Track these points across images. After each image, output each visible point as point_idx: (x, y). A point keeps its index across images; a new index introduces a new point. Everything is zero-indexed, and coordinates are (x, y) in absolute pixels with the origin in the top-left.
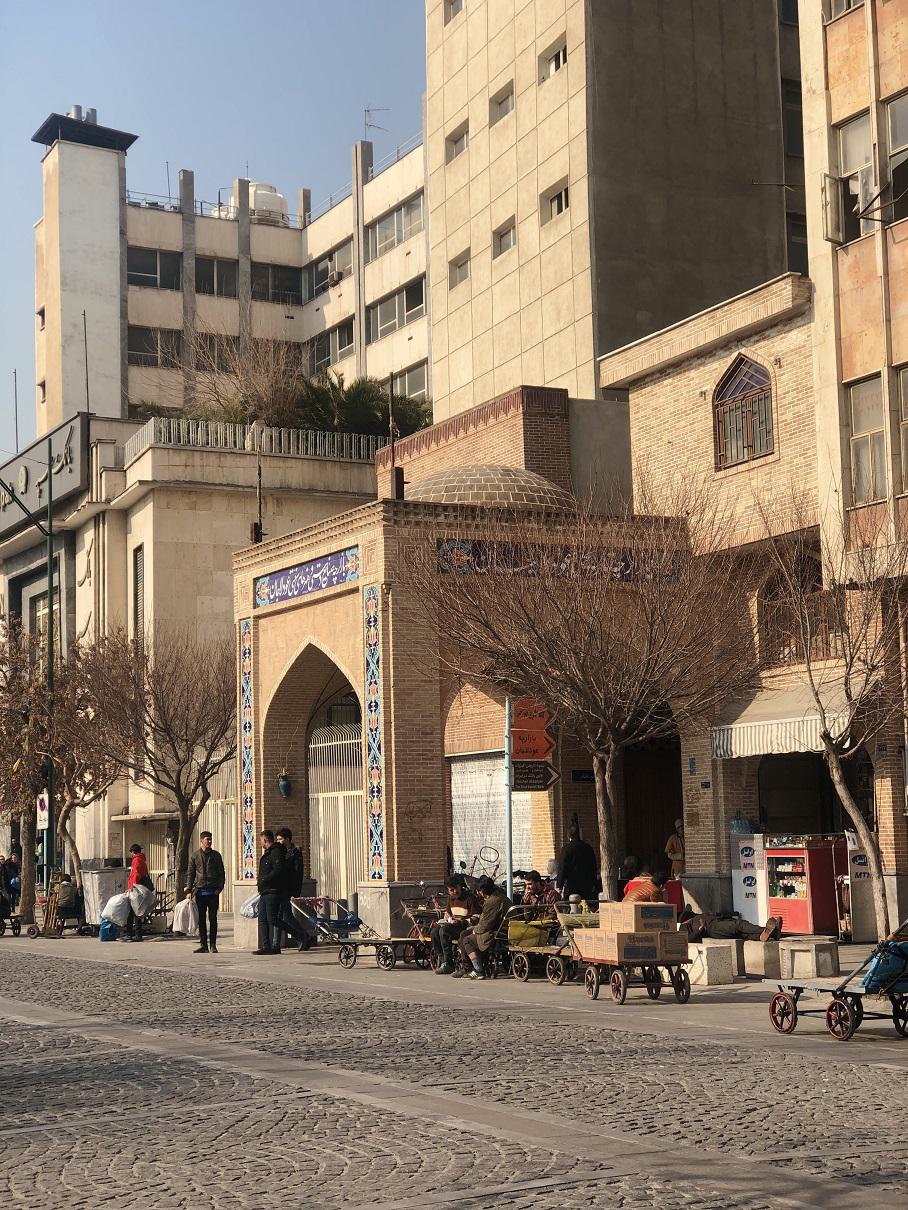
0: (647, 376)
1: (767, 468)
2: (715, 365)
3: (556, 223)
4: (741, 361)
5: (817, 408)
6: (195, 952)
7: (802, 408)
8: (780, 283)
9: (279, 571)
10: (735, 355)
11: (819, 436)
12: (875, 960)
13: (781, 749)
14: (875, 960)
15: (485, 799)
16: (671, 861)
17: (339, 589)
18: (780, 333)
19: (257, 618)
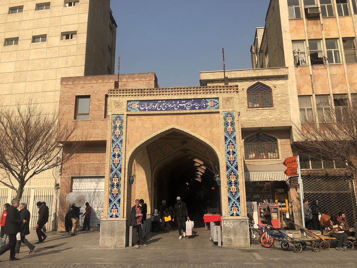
0: (216, 80)
1: (270, 110)
2: (248, 83)
3: (70, 41)
4: (258, 83)
5: (290, 99)
6: (162, 238)
7: (284, 98)
8: (284, 68)
9: (152, 100)
10: (258, 81)
11: (291, 106)
12: (151, 239)
13: (270, 180)
14: (151, 239)
15: (94, 191)
16: (141, 213)
17: (203, 111)
18: (275, 80)
19: (128, 115)
